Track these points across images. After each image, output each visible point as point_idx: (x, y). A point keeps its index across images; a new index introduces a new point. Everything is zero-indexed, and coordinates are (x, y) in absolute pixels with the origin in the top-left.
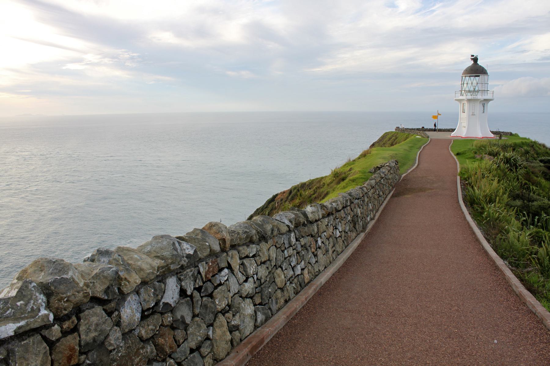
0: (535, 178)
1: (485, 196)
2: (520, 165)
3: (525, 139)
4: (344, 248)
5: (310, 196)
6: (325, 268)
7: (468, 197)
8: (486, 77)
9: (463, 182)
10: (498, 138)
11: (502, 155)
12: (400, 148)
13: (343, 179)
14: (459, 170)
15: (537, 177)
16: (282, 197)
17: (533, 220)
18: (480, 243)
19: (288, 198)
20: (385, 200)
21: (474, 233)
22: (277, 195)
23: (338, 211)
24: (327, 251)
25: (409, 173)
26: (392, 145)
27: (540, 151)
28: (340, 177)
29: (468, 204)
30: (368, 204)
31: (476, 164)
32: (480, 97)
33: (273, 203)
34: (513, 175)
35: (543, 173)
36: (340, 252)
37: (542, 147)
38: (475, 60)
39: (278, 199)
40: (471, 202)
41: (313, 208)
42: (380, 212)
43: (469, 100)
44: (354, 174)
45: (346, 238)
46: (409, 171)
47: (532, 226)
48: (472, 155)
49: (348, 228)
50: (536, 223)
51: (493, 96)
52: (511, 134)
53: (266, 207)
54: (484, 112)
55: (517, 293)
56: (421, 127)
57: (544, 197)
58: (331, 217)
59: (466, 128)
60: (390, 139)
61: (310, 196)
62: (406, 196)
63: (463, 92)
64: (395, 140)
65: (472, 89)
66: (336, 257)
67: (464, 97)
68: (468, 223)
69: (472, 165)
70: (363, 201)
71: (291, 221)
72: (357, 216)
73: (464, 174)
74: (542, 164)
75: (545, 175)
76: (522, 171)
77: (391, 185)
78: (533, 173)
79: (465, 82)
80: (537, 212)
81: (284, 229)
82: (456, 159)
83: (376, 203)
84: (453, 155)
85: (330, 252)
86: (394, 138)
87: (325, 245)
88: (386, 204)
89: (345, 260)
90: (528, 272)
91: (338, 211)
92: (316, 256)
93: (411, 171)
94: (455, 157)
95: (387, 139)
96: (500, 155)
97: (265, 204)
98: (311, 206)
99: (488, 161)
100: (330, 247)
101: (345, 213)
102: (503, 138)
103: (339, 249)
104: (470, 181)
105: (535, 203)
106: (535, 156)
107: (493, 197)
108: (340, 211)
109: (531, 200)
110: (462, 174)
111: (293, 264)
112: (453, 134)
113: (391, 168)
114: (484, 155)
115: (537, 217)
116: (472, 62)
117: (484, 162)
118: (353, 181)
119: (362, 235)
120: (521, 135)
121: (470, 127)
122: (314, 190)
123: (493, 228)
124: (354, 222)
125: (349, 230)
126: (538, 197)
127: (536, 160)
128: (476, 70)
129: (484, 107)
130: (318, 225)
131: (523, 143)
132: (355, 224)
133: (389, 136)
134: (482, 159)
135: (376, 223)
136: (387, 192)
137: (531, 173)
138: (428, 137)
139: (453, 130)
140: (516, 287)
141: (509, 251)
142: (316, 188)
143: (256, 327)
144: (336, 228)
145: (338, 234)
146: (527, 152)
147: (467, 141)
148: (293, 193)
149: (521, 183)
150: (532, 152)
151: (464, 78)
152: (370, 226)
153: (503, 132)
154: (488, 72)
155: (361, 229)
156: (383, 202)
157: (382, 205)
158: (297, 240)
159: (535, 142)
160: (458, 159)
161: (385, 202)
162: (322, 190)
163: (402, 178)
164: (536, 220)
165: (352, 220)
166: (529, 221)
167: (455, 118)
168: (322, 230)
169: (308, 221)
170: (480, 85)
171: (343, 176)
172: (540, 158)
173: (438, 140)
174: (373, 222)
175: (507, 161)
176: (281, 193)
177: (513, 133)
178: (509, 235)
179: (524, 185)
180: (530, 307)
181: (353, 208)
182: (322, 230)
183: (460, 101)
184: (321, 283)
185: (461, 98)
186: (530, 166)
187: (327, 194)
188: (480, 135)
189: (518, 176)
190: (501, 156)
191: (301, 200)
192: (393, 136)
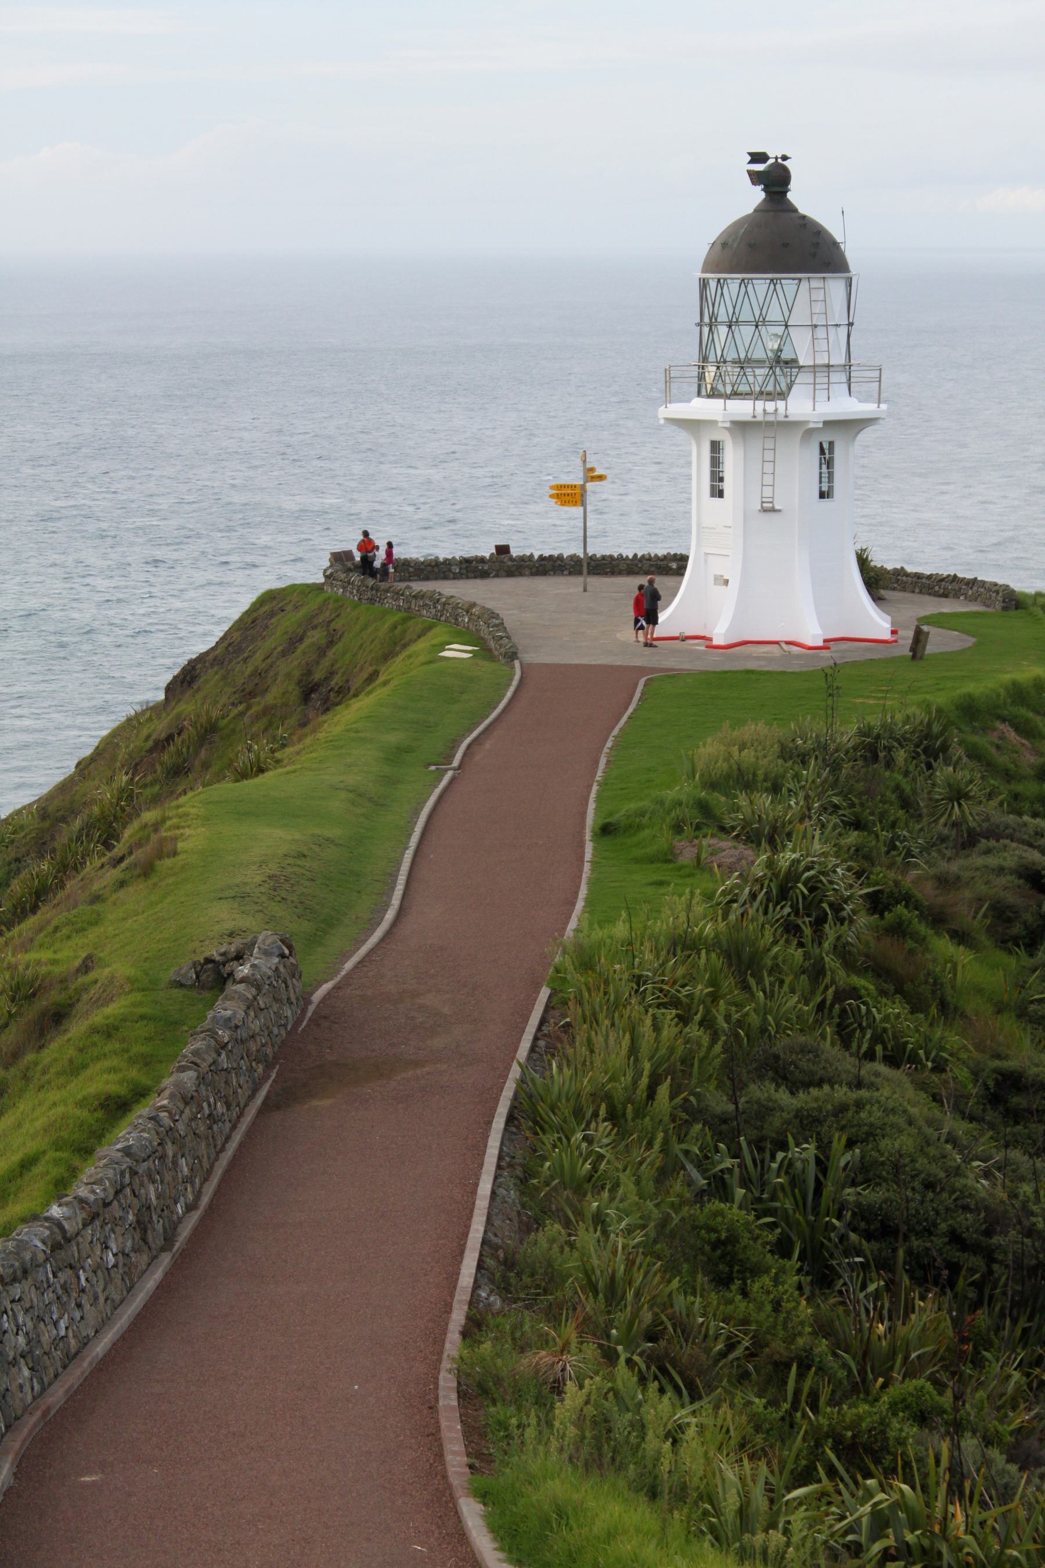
4: (125, 1292)
6: (96, 1332)
8: (835, 286)
13: (58, 1017)
20: (234, 1127)
23: (106, 1204)
24: (96, 1298)
25: (349, 975)
28: (43, 1003)
30: (175, 1163)
32: (802, 405)
36: (117, 1301)
38: (774, 179)
41: (65, 1209)
42: (215, 1180)
43: (742, 428)
45: (126, 1269)
46: (349, 965)
49: (129, 1244)
56: (487, 551)
58: (97, 1223)
60: (294, 641)
62: (315, 1103)
64: (321, 653)
66: (112, 1314)
70: (163, 1158)
71: (44, 1242)
72: (149, 1208)
81: (41, 1257)
82: (588, 856)
83: (203, 1149)
85: (102, 1299)
86: (316, 636)
87: (92, 1286)
88: (241, 1145)
89: (132, 1319)
91: (106, 1204)
92: (79, 1306)
95: (273, 641)
98: (59, 1206)
100: (99, 1290)
101: (120, 1205)
103: (117, 1298)
108: (110, 1204)
111: (54, 1317)
113: (259, 988)
116: (757, 195)
118: (109, 1032)
121: (766, 584)
124: (142, 1226)
125: (134, 1250)
128: (780, 241)
130: (78, 1245)
132: (146, 1231)
133: (288, 622)
135: (202, 1220)
136: (242, 1095)
143: (34, 1398)
144: (107, 1247)
145: (111, 1260)
152: (185, 1232)
155: (160, 1242)
156: (228, 1138)
157: (223, 1149)
158: (55, 1276)
161: (237, 1137)
165: (138, 1222)
168: (84, 1255)
169: (65, 1237)
171: (55, 996)
174: (195, 1216)
181: (136, 1187)
182: (84, 1255)
184: (97, 1354)
192: (310, 623)
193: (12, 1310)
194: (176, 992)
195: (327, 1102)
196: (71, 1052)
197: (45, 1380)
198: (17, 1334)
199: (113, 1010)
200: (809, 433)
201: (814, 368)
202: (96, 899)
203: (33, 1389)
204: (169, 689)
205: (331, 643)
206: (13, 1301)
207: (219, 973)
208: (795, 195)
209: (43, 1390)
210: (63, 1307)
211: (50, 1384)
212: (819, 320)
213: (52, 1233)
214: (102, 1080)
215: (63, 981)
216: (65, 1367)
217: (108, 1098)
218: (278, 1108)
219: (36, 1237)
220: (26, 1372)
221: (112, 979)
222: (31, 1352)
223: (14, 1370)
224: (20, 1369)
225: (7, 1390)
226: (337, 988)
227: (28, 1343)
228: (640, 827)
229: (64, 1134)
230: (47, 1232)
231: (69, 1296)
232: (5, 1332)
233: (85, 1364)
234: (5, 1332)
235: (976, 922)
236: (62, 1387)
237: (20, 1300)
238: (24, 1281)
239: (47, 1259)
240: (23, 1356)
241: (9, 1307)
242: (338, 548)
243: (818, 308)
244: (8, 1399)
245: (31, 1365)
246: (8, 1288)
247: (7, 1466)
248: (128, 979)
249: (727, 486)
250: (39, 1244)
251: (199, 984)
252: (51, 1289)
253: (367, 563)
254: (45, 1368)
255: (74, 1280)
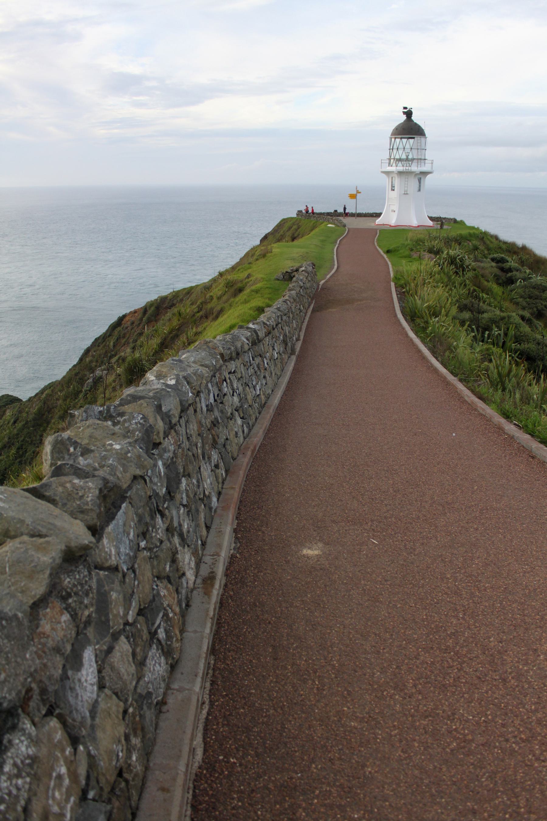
0: (486, 283)
1: (429, 307)
2: (467, 267)
3: (473, 228)
5: (194, 315)
7: (408, 310)
8: (423, 139)
9: (399, 289)
10: (439, 226)
11: (445, 252)
12: (308, 244)
13: (240, 290)
14: (392, 275)
15: (488, 281)
16: (133, 319)
17: (483, 336)
18: (428, 361)
19: (141, 320)
21: (419, 351)
22: (124, 316)
24: (271, 373)
25: (329, 279)
26: (293, 239)
27: (491, 246)
28: (236, 287)
29: (408, 318)
31: (414, 266)
32: (414, 168)
33: (119, 329)
34: (459, 280)
35: (495, 276)
37: (494, 240)
38: (409, 114)
39: (126, 323)
40: (412, 316)
43: (400, 173)
44: (255, 283)
46: (328, 276)
47: (481, 343)
48: (407, 253)
50: (486, 339)
51: (432, 167)
52: (455, 221)
53: (110, 336)
54: (419, 190)
55: (469, 402)
56: (332, 211)
57: (495, 307)
59: (396, 212)
60: (290, 228)
61: (194, 315)
62: (330, 310)
63: (392, 161)
64: (297, 230)
65: (404, 157)
67: (393, 169)
68: (411, 340)
69: (409, 268)
71: (248, 340)
73: (399, 279)
74: (494, 264)
75: (498, 279)
76: (470, 274)
77: (310, 297)
78: (483, 276)
79: (395, 147)
80: (488, 326)
81: (246, 347)
82: (387, 259)
84: (382, 253)
85: (273, 374)
86: (295, 227)
88: (309, 321)
90: (479, 385)
92: (265, 377)
93: (331, 277)
94: (385, 256)
95: (285, 228)
96: (442, 252)
97: (107, 331)
99: (428, 263)
102: (445, 227)
104: (408, 288)
105: (485, 315)
106: (486, 252)
107: (438, 309)
109: (481, 312)
110: (396, 279)
112: (379, 221)
114: (423, 253)
115: (487, 332)
116: (404, 117)
117: (424, 263)
118: (257, 291)
119: (294, 358)
120: (469, 223)
121: (401, 212)
122: (198, 307)
123: (439, 345)
126: (489, 308)
127: (486, 258)
128: (410, 129)
129: (420, 182)
131: (470, 235)
133: (289, 224)
134: (420, 258)
136: (307, 305)
137: (480, 277)
138: (345, 226)
139: (378, 215)
140: (468, 397)
141: (459, 368)
142: (201, 303)
143: (245, 438)
146: (476, 248)
147: (399, 231)
148: (150, 312)
149: (469, 289)
150: (482, 247)
151: (393, 140)
153: (445, 218)
154: (426, 132)
156: (304, 319)
157: (303, 322)
158: (253, 360)
159: (485, 233)
160: (389, 258)
162: (209, 306)
163: (320, 287)
164: (486, 336)
166: (479, 337)
167: (381, 197)
169: (258, 339)
170: (415, 152)
171: (239, 285)
172: (492, 256)
173: (358, 230)
175: (452, 261)
176: (131, 312)
177: (458, 219)
178: (458, 350)
179: (473, 293)
180: (481, 411)
183: (387, 173)
185: (389, 169)
186: (479, 267)
187: (221, 312)
188: (415, 223)
189: (465, 281)
190: (444, 255)
191: (181, 321)
192: (293, 224)
193: (230, 379)
194: (277, 281)
195: (333, 310)
196: (245, 297)
197: (251, 423)
198: (233, 395)
199: (259, 285)
200: (416, 175)
201: (418, 159)
202: (250, 263)
203: (243, 432)
204: (261, 241)
205: (299, 228)
206: (230, 373)
207: (290, 276)
208: (413, 118)
209: (250, 430)
210: (258, 377)
211: (253, 426)
212: (419, 148)
213: (252, 335)
214: (258, 302)
215: (241, 281)
216: (260, 413)
217: (259, 307)
218: (318, 311)
219: (244, 337)
220: (239, 421)
221: (256, 279)
222: (242, 406)
223: (232, 422)
224: (235, 420)
225: (227, 439)
226: (326, 282)
227: (240, 401)
228: (398, 251)
229: (245, 318)
230: (249, 334)
231: (260, 371)
232: (225, 395)
233: (271, 411)
234: (225, 395)
235: (491, 277)
236: (261, 428)
237: (234, 372)
238: (237, 360)
239: (249, 349)
240: (237, 410)
241: (227, 376)
242: (300, 209)
243: (419, 144)
244: (228, 447)
245: (242, 416)
246: (227, 364)
247: (231, 516)
248: (262, 278)
249: (396, 189)
250: (245, 340)
251: (284, 279)
252: (252, 367)
253: (307, 211)
254: (250, 416)
255: (262, 363)
